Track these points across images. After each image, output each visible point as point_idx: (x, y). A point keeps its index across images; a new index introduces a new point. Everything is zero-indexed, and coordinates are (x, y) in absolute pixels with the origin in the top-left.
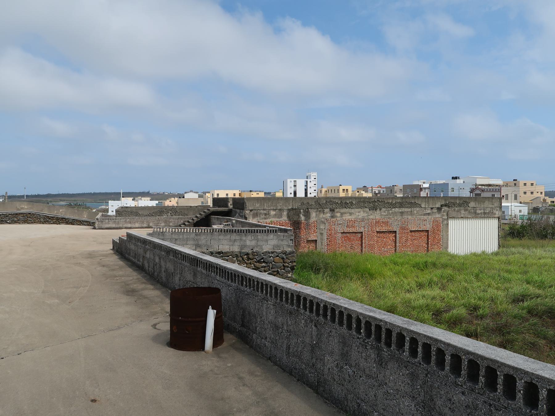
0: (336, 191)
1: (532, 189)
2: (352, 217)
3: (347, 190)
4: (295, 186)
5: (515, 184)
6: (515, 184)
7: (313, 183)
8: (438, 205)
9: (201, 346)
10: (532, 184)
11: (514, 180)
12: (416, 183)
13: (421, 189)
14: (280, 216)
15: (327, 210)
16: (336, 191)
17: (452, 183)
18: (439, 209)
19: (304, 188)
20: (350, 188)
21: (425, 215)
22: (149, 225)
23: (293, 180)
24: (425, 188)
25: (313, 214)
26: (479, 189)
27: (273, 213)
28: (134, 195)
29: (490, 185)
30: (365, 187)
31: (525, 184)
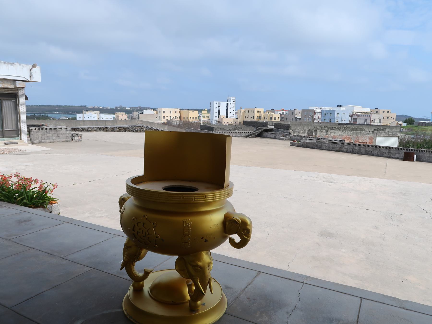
0: (252, 112)
1: (388, 115)
2: (335, 135)
3: (260, 111)
4: (219, 107)
5: (377, 112)
6: (377, 112)
7: (232, 105)
8: (373, 130)
9: (413, 161)
10: (388, 112)
11: (376, 109)
12: (311, 108)
13: (315, 113)
14: (305, 133)
15: (324, 131)
16: (252, 112)
17: (337, 109)
18: (373, 132)
19: (226, 108)
20: (262, 110)
21: (366, 134)
22: (275, 137)
23: (218, 102)
24: (318, 113)
25: (319, 133)
26: (356, 115)
27: (301, 131)
28: (104, 111)
29: (364, 113)
30: (272, 109)
31: (384, 112)
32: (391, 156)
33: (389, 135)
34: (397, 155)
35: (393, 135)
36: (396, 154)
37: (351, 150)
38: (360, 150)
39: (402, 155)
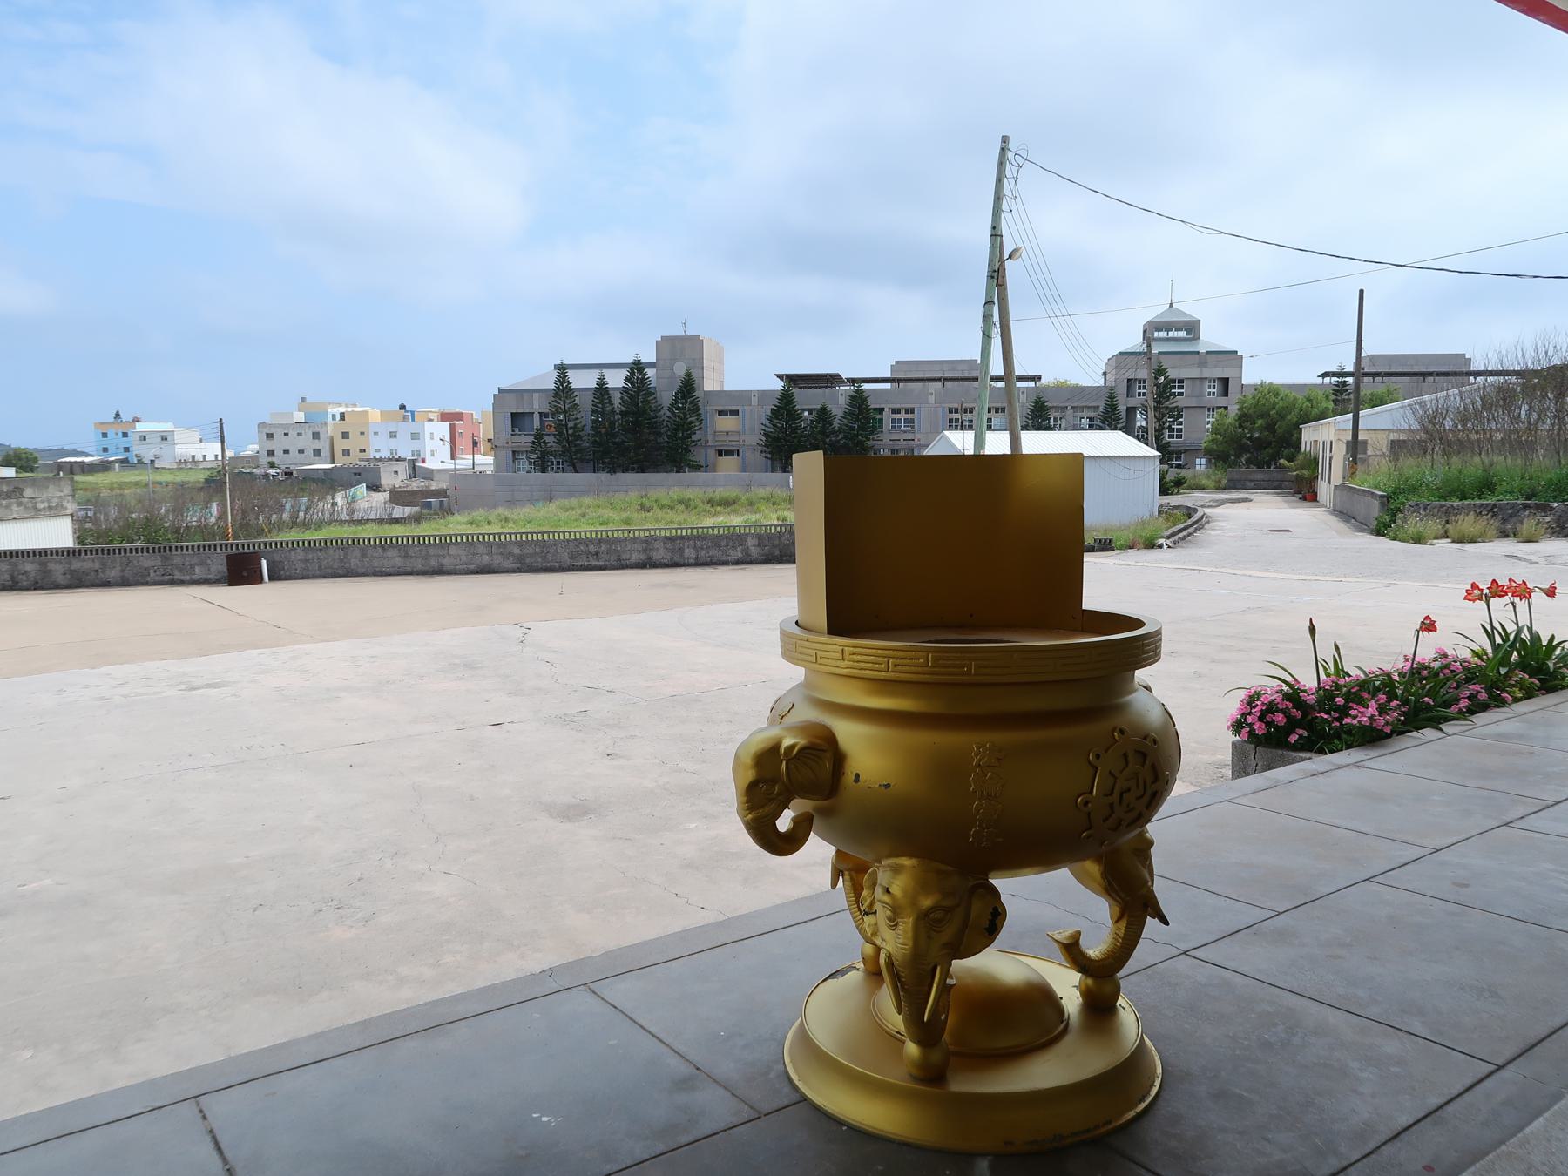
32: (178, 576)
33: (36, 513)
34: (197, 569)
35: (53, 511)
36: (192, 567)
37: (7, 577)
38: (46, 572)
39: (219, 565)
